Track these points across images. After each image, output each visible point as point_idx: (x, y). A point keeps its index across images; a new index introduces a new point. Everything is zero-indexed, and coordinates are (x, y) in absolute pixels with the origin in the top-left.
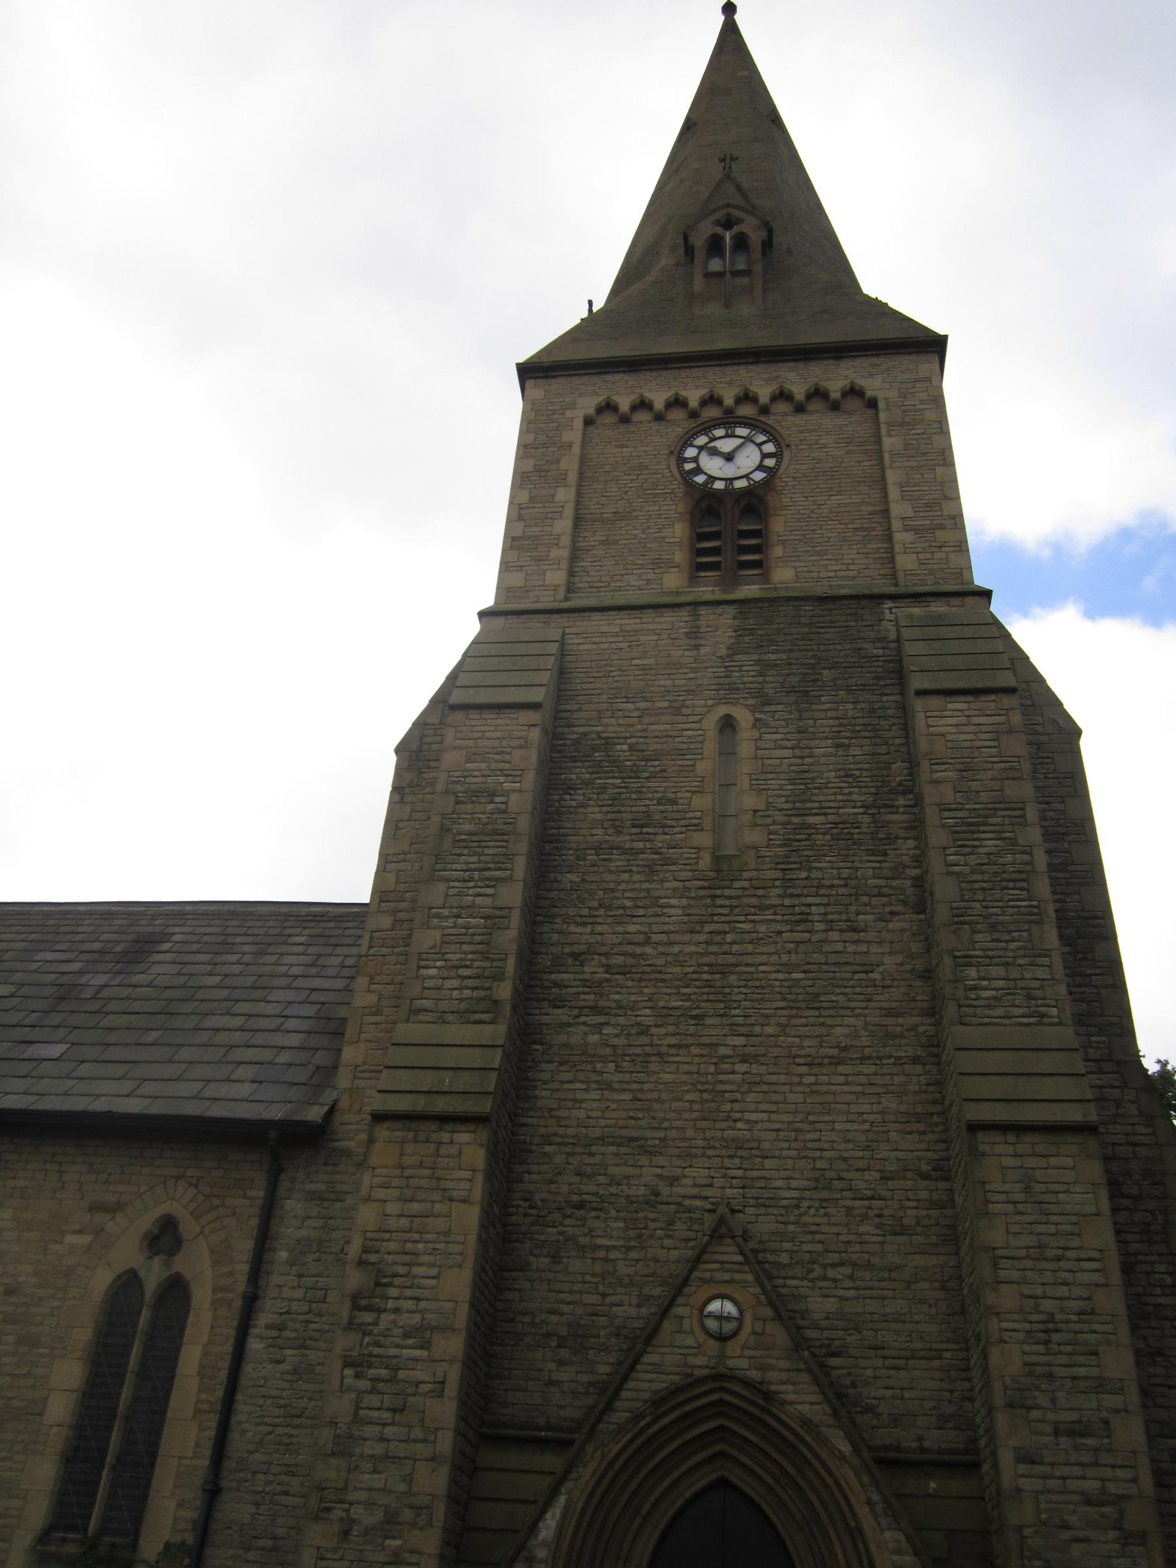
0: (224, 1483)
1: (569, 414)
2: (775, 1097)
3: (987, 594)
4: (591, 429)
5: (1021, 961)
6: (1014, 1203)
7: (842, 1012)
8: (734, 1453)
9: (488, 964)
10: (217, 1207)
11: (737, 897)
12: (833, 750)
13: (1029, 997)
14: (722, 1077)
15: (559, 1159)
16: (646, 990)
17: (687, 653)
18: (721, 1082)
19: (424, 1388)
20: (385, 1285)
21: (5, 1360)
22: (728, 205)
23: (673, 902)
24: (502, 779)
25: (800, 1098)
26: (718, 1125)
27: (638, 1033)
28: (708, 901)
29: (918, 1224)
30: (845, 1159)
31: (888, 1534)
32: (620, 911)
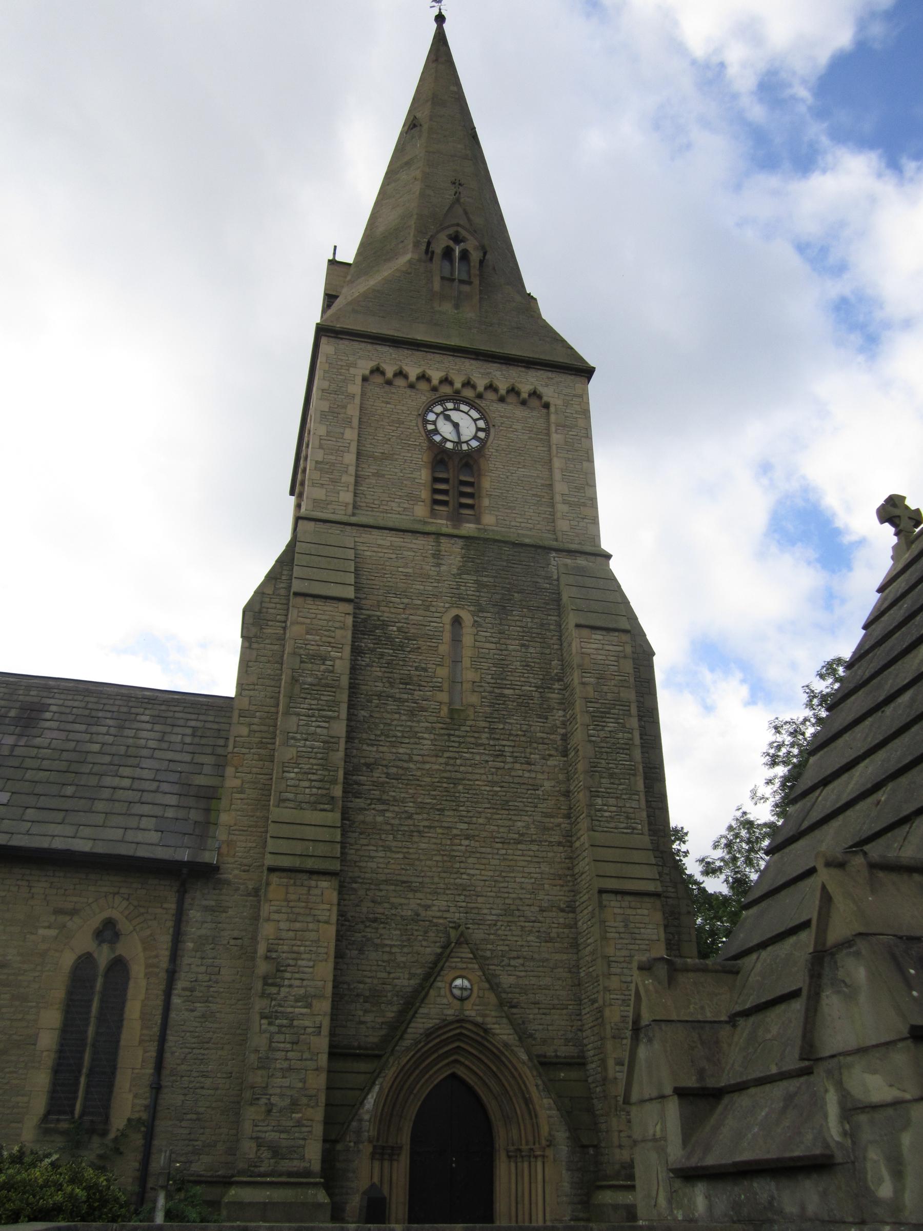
0: (163, 1083)
1: (352, 371)
2: (484, 861)
3: (608, 557)
4: (366, 384)
5: (624, 797)
6: (619, 933)
7: (521, 813)
8: (462, 1060)
9: (326, 773)
10: (143, 914)
11: (463, 737)
12: (518, 648)
13: (628, 818)
14: (454, 848)
15: (361, 893)
16: (410, 791)
17: (433, 568)
18: (454, 850)
19: (309, 1030)
20: (282, 971)
21: (4, 1010)
22: (458, 225)
23: (426, 736)
24: (330, 649)
25: (497, 862)
26: (452, 876)
27: (406, 818)
28: (446, 737)
29: (558, 937)
30: (521, 899)
31: (545, 1101)
32: (394, 739)
